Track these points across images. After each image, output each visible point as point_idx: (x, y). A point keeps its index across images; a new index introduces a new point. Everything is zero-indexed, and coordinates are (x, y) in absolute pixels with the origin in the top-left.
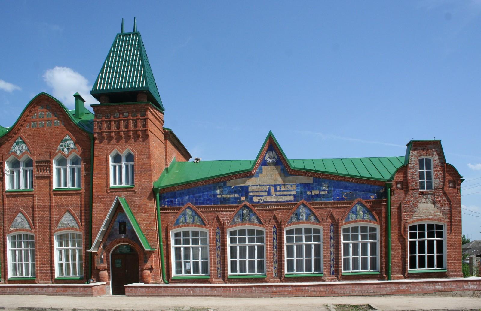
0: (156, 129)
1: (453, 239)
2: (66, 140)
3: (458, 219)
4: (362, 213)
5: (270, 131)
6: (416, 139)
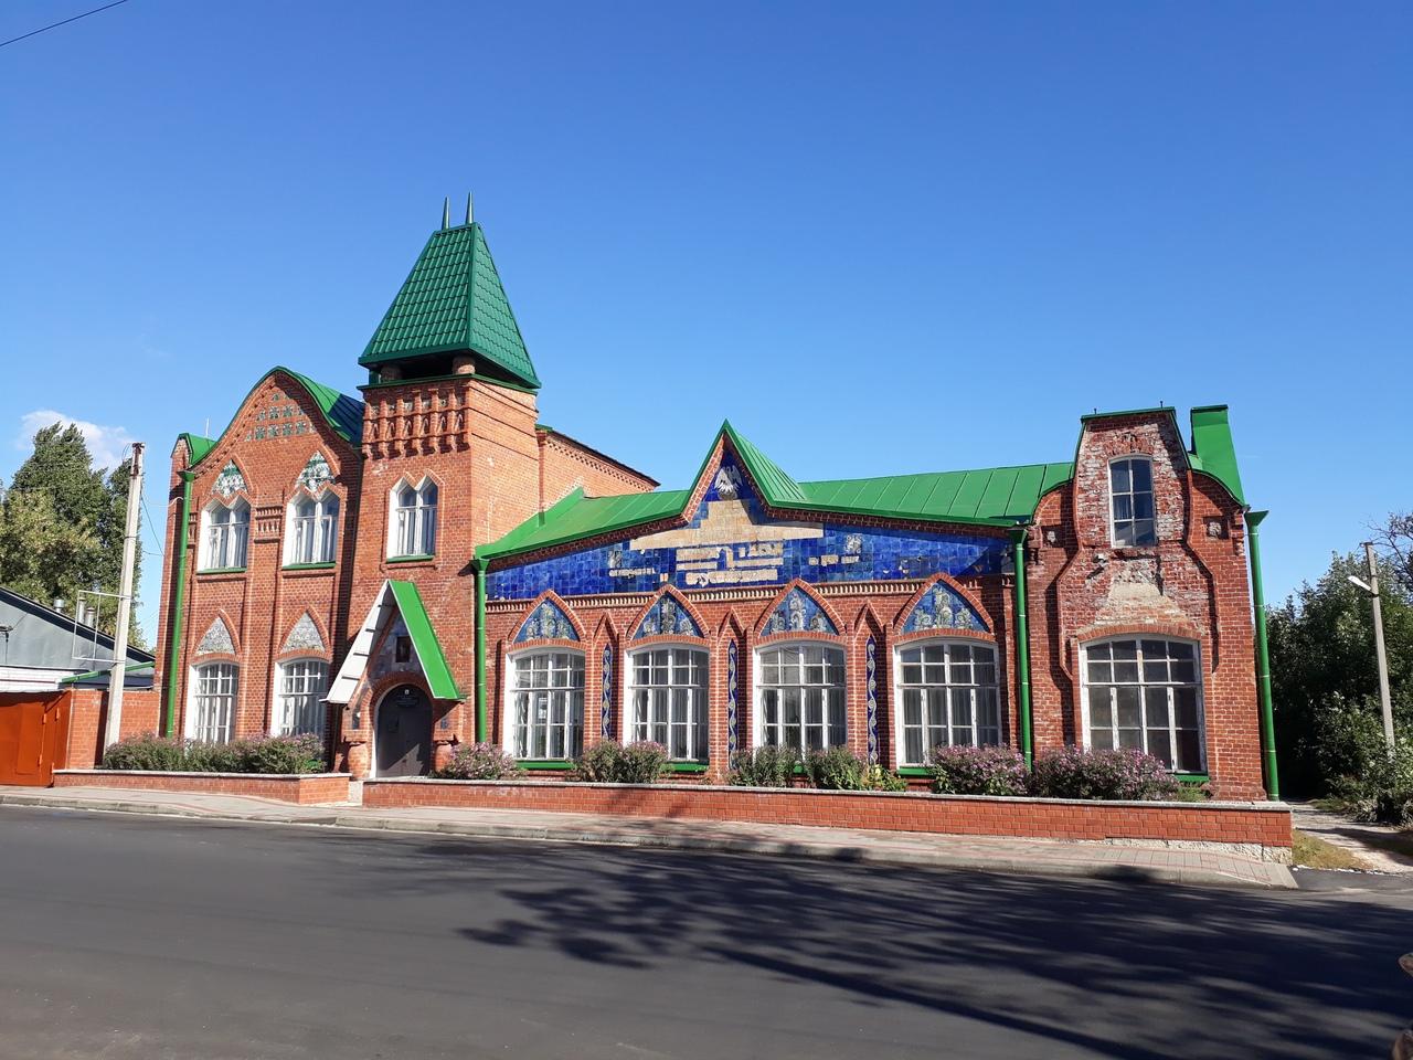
1: (1226, 685)
2: (315, 463)
3: (1243, 628)
4: (950, 611)
5: (726, 422)
6: (1102, 411)
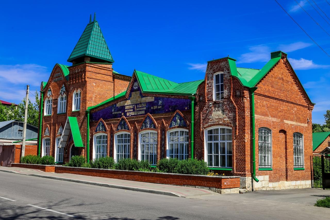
0: (107, 77)
1: (238, 141)
2: (63, 87)
4: (179, 121)
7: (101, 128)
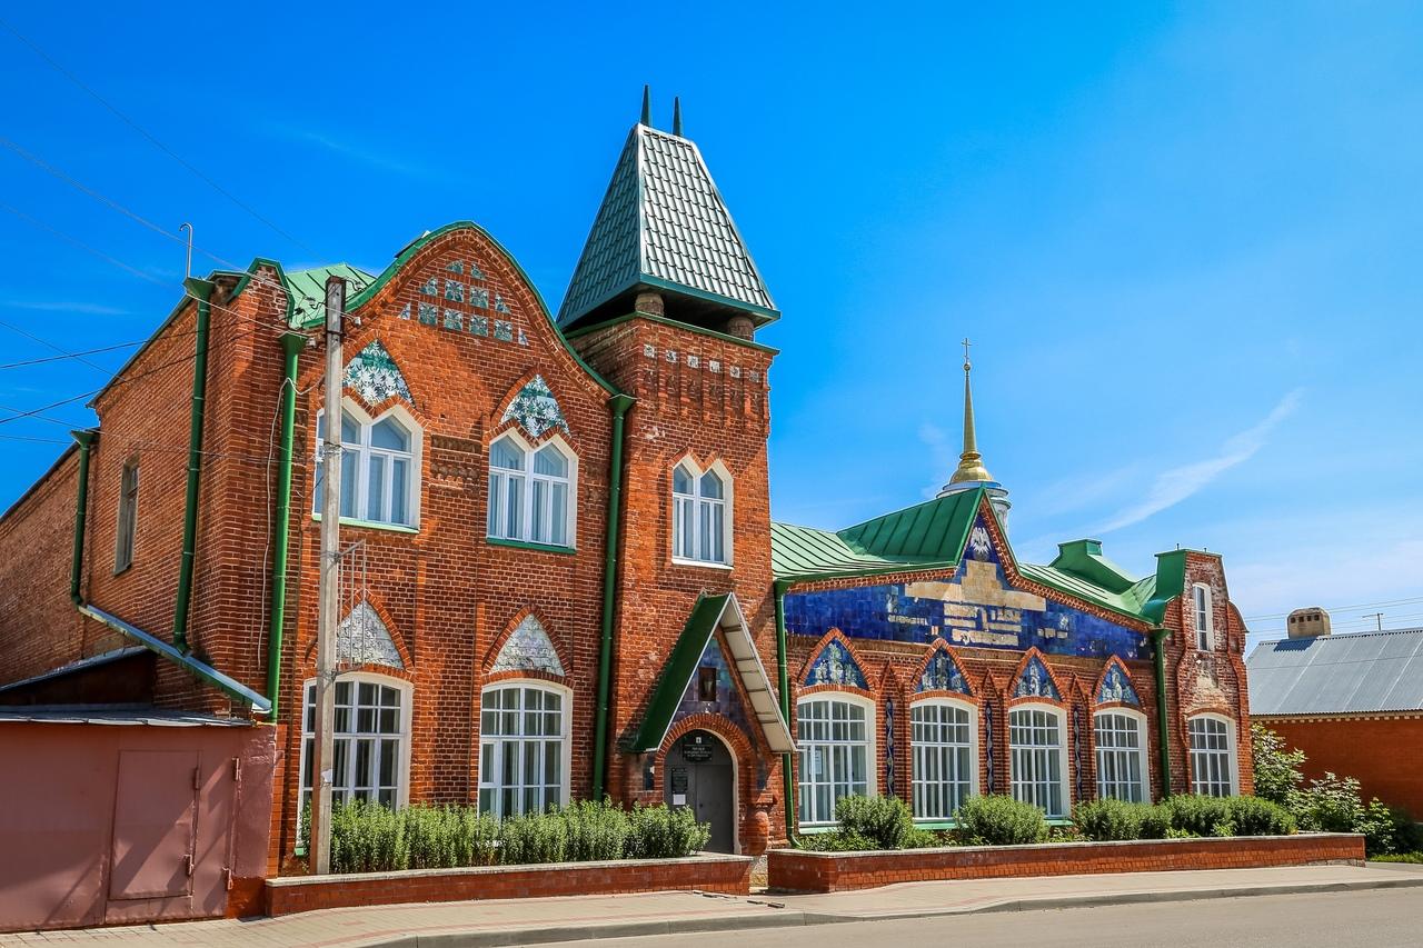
7: (836, 673)
